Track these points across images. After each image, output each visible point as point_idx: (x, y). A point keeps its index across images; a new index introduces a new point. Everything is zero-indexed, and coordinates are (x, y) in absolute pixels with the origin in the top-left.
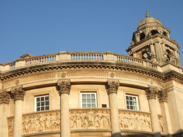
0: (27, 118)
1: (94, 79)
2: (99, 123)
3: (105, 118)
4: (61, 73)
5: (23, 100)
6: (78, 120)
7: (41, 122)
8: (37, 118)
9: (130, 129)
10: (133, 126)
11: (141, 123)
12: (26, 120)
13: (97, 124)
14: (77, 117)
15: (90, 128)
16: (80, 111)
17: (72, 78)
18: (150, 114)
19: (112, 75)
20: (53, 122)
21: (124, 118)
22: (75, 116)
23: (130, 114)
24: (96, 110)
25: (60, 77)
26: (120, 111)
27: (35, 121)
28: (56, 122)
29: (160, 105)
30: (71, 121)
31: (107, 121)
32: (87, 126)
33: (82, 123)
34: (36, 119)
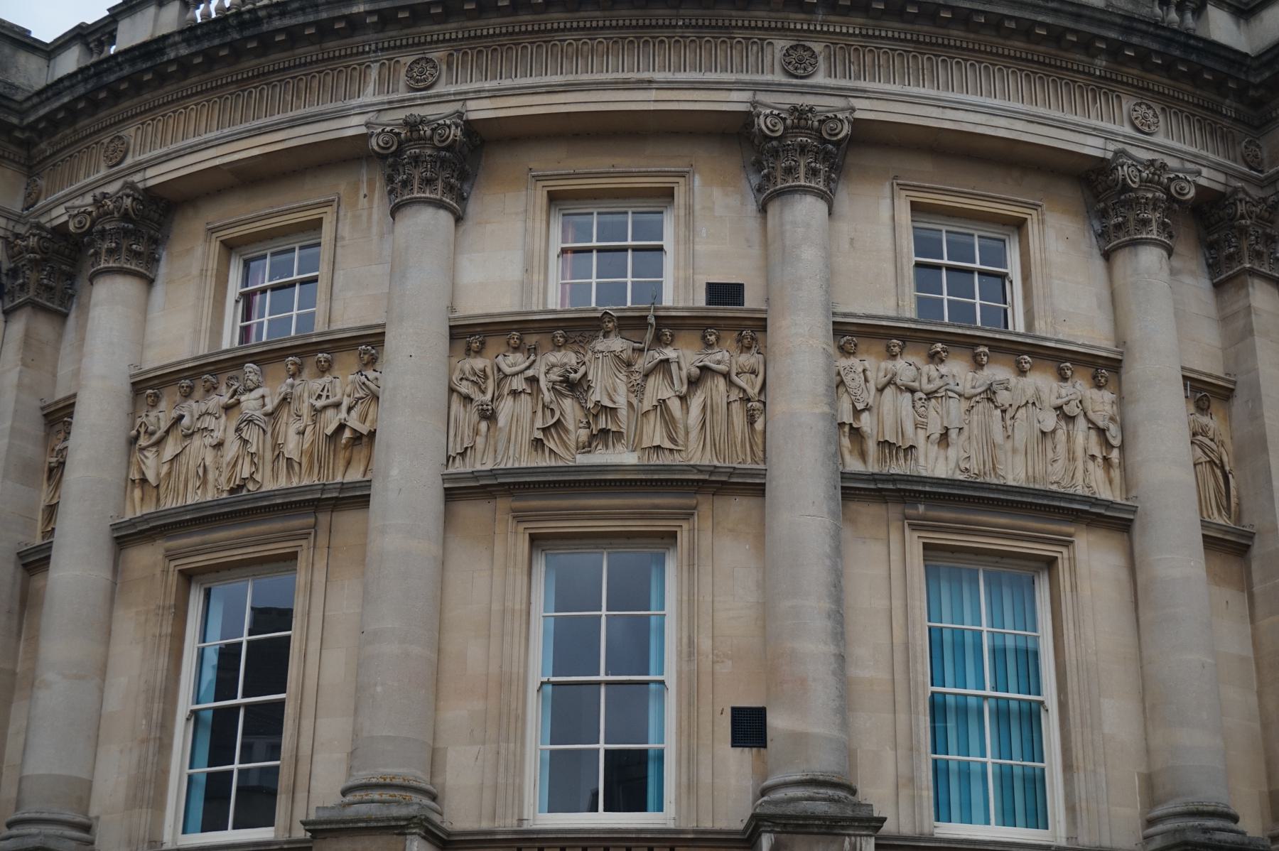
0: (163, 405)
1: (653, 95)
3: (721, 382)
4: (403, 60)
5: (150, 282)
6: (510, 400)
7: (250, 421)
8: (225, 399)
9: (924, 474)
11: (1023, 431)
13: (655, 433)
15: (602, 457)
16: (531, 340)
19: (798, 64)
20: (331, 421)
21: (881, 390)
22: (489, 371)
23: (934, 358)
24: (669, 326)
25: (977, 811)
26: (850, 334)
27: (208, 422)
28: (354, 421)
29: (1220, 307)
30: (456, 405)
31: (736, 407)
32: (572, 445)
33: (539, 424)
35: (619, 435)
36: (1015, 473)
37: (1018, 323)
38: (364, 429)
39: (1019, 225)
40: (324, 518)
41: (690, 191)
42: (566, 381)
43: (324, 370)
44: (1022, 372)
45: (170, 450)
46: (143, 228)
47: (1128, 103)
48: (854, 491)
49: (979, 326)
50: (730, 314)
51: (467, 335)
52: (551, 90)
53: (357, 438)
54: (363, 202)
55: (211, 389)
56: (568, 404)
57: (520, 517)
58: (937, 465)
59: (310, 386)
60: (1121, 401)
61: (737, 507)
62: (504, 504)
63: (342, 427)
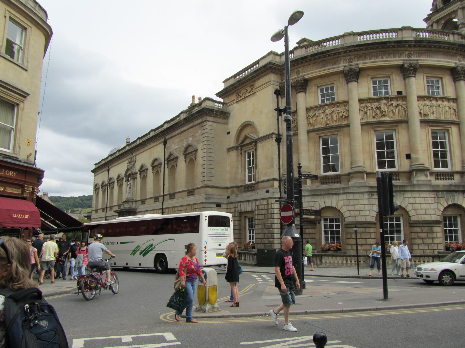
1: (388, 62)
2: (393, 113)
5: (306, 93)
8: (323, 111)
10: (435, 115)
12: (310, 114)
14: (367, 107)
15: (384, 119)
16: (371, 101)
17: (360, 64)
18: (456, 99)
24: (392, 98)
27: (320, 115)
28: (345, 114)
34: (321, 111)
35: (386, 115)
36: (442, 118)
37: (441, 94)
38: (347, 115)
39: (441, 78)
40: (342, 129)
41: (393, 77)
42: (377, 108)
43: (338, 107)
44: (443, 102)
45: (314, 119)
46: (303, 86)
47: (458, 57)
48: (422, 122)
49: (435, 95)
50: (401, 96)
51: (361, 101)
52: (372, 62)
53: (345, 117)
54: (341, 79)
55: (319, 110)
56: (378, 111)
57: (373, 128)
58: (432, 117)
59: (336, 109)
60: (457, 105)
61: (404, 125)
62: (369, 126)
63: (343, 115)
